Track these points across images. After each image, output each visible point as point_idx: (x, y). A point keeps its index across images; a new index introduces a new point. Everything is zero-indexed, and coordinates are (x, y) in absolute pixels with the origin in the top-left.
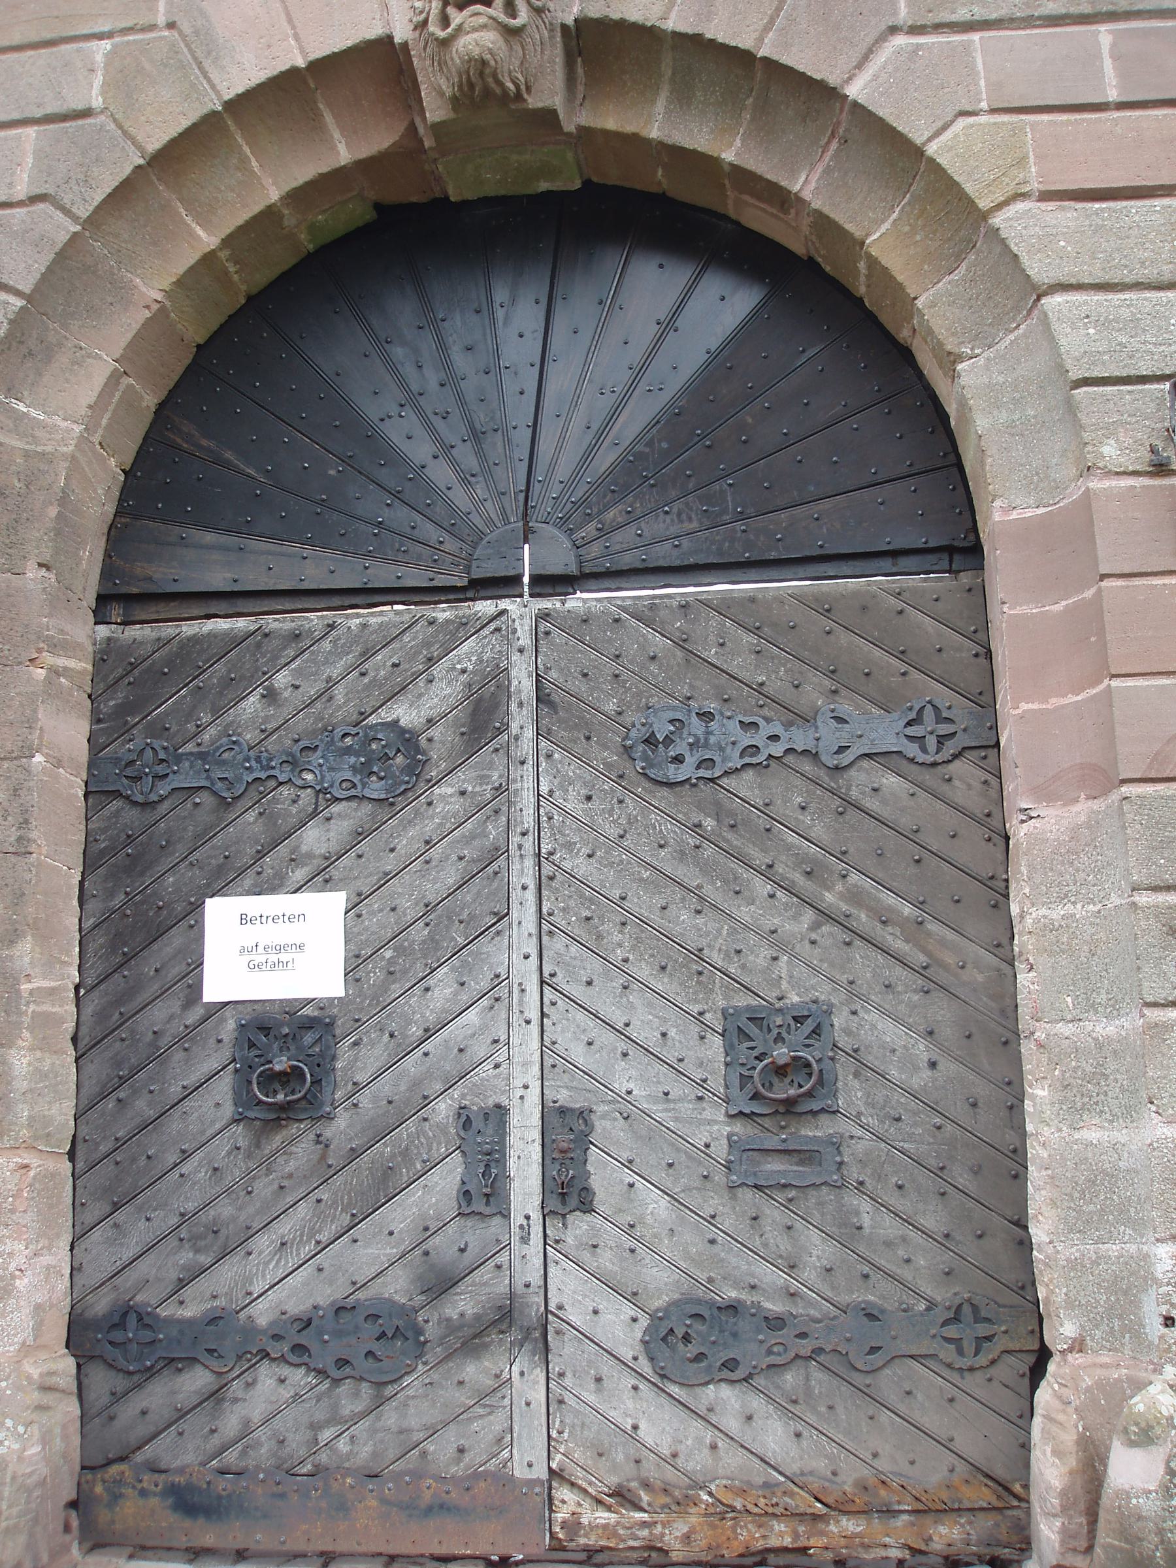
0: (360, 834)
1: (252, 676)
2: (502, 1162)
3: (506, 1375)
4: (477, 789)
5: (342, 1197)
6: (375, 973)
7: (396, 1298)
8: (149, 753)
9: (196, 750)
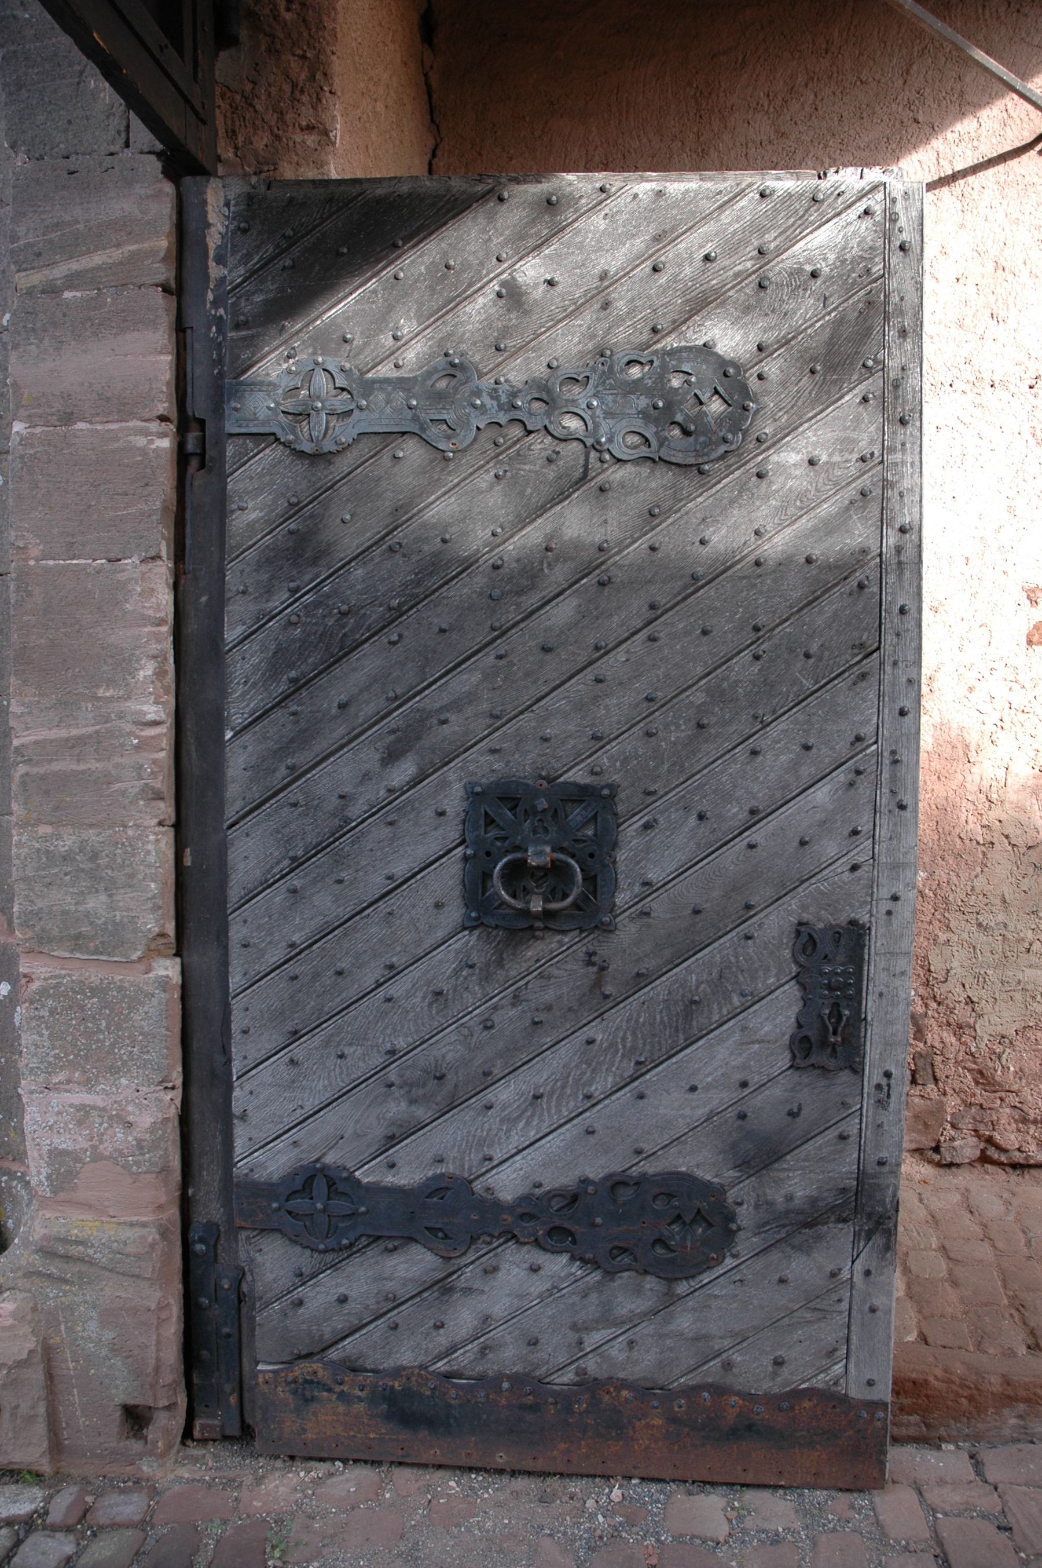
0: (498, 717)
1: (482, 264)
2: (857, 1001)
3: (845, 1275)
4: (836, 458)
5: (624, 1039)
6: (678, 726)
7: (699, 1173)
8: (321, 380)
9: (396, 374)
